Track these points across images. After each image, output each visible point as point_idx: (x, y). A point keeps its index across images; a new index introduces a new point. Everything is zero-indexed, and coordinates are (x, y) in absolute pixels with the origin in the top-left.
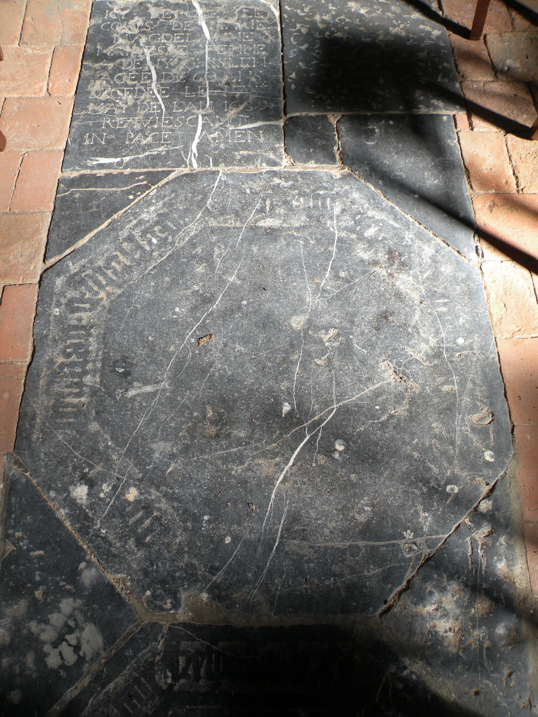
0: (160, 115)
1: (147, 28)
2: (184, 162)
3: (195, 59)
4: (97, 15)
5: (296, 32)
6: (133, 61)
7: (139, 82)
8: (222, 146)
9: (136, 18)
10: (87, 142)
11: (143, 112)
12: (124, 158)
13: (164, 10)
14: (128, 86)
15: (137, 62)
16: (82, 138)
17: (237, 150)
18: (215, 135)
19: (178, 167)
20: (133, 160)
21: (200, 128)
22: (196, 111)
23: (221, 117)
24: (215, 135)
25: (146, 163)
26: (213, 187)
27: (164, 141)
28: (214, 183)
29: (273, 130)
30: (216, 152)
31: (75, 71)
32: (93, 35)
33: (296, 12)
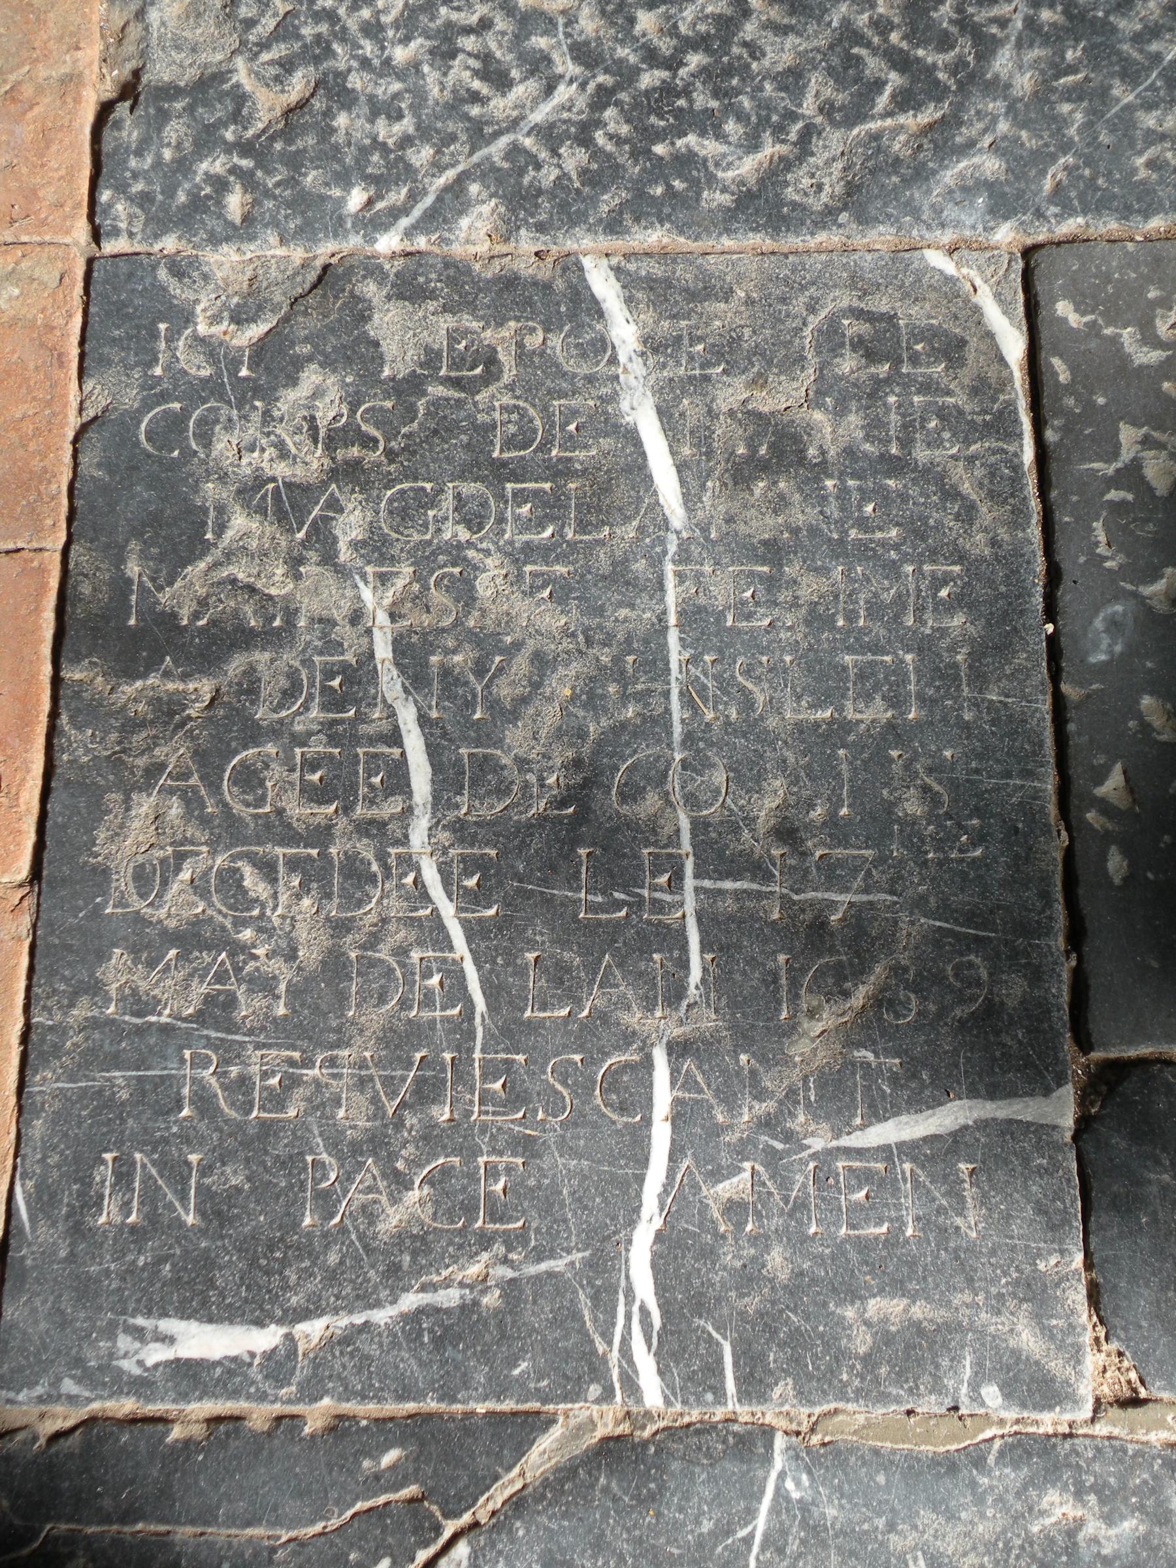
0: (462, 1029)
1: (368, 442)
2: (596, 1369)
3: (617, 660)
4: (115, 354)
5: (1114, 482)
6: (307, 663)
7: (347, 809)
8: (777, 1259)
9: (311, 377)
10: (108, 1215)
11: (376, 1017)
12: (301, 1328)
13: (446, 322)
14: (290, 837)
15: (329, 674)
16: (86, 1181)
17: (854, 1295)
18: (736, 1186)
19: (565, 1398)
20: (347, 1339)
21: (661, 1136)
22: (633, 1018)
23: (763, 1059)
24: (736, 1186)
25: (409, 1364)
26: (748, 1541)
27: (494, 1215)
28: (750, 1514)
29: (1026, 1161)
30: (752, 1303)
31: (25, 721)
32: (105, 489)
33: (1115, 340)
